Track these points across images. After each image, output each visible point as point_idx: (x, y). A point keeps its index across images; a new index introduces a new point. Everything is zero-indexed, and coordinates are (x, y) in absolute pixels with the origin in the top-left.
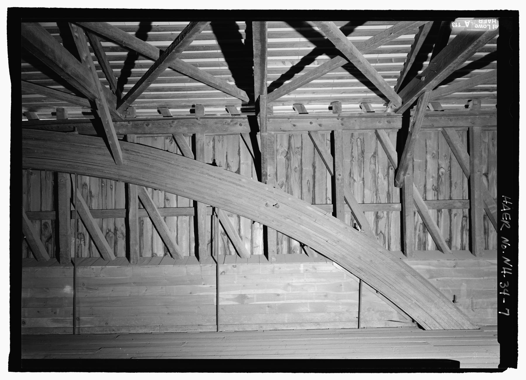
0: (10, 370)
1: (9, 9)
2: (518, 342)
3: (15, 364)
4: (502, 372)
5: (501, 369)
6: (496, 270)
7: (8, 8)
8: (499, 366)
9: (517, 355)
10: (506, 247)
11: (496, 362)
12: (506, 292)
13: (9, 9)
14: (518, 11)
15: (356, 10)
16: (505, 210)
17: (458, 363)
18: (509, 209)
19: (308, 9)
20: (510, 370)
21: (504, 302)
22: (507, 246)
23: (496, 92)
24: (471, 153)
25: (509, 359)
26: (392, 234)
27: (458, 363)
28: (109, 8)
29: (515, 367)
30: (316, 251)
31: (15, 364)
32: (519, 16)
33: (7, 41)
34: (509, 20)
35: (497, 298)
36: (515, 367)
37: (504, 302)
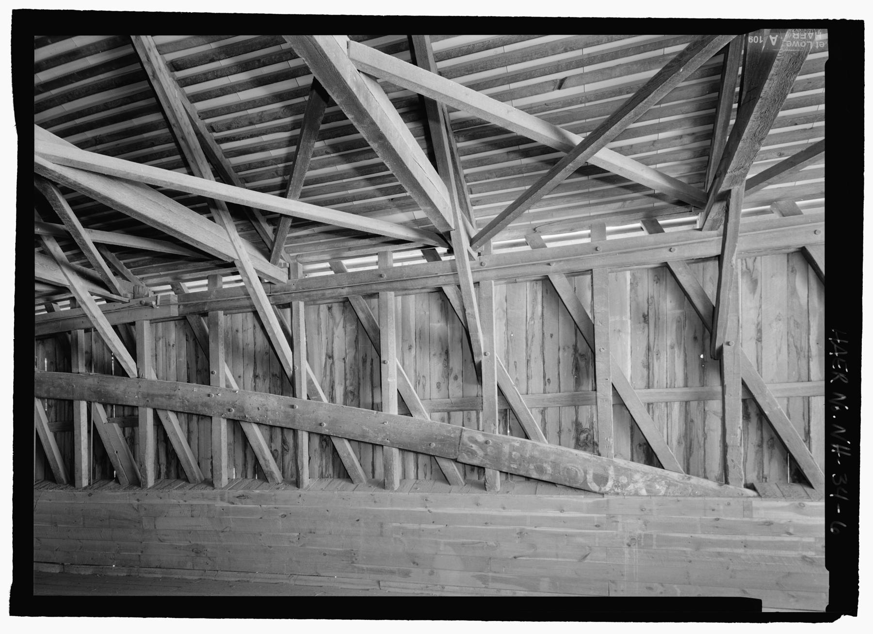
0: (12, 613)
1: (15, 12)
3: (24, 602)
4: (832, 621)
5: (829, 616)
6: (824, 523)
7: (14, 11)
9: (857, 594)
11: (821, 604)
13: (15, 12)
17: (758, 603)
18: (846, 353)
19: (513, 16)
20: (845, 619)
21: (839, 511)
22: (842, 408)
23: (822, 107)
24: (439, 165)
25: (843, 599)
26: (677, 371)
27: (758, 603)
29: (855, 614)
31: (24, 602)
33: (10, 65)
34: (847, 37)
35: (824, 518)
36: (855, 614)
37: (839, 511)
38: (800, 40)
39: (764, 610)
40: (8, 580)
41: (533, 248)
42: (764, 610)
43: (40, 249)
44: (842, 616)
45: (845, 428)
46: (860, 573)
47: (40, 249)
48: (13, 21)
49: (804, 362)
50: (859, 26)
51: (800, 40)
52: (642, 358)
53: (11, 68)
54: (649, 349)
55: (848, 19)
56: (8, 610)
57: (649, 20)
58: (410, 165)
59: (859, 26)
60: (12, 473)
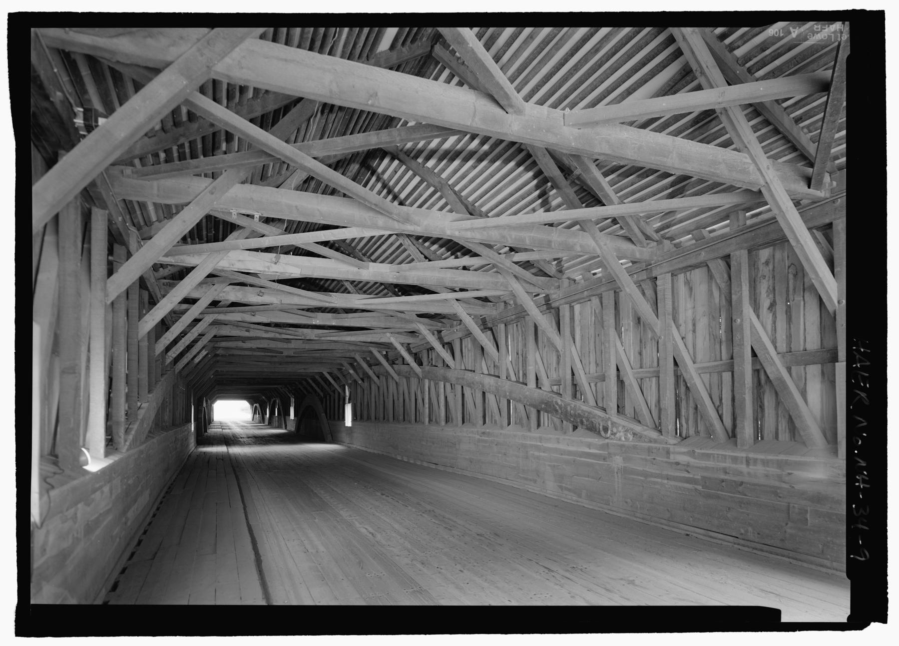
1: (11, 15)
2: (888, 578)
4: (862, 629)
9: (886, 601)
13: (11, 15)
17: (777, 613)
19: (523, 11)
20: (874, 626)
25: (869, 606)
29: (884, 620)
33: (7, 70)
34: (868, 29)
36: (884, 620)
39: (783, 621)
41: (633, 262)
44: (872, 623)
48: (9, 24)
49: (718, 346)
50: (879, 17)
52: (736, 361)
53: (7, 74)
54: (641, 342)
55: (868, 9)
56: (14, 630)
57: (664, 13)
58: (821, 275)
59: (879, 17)
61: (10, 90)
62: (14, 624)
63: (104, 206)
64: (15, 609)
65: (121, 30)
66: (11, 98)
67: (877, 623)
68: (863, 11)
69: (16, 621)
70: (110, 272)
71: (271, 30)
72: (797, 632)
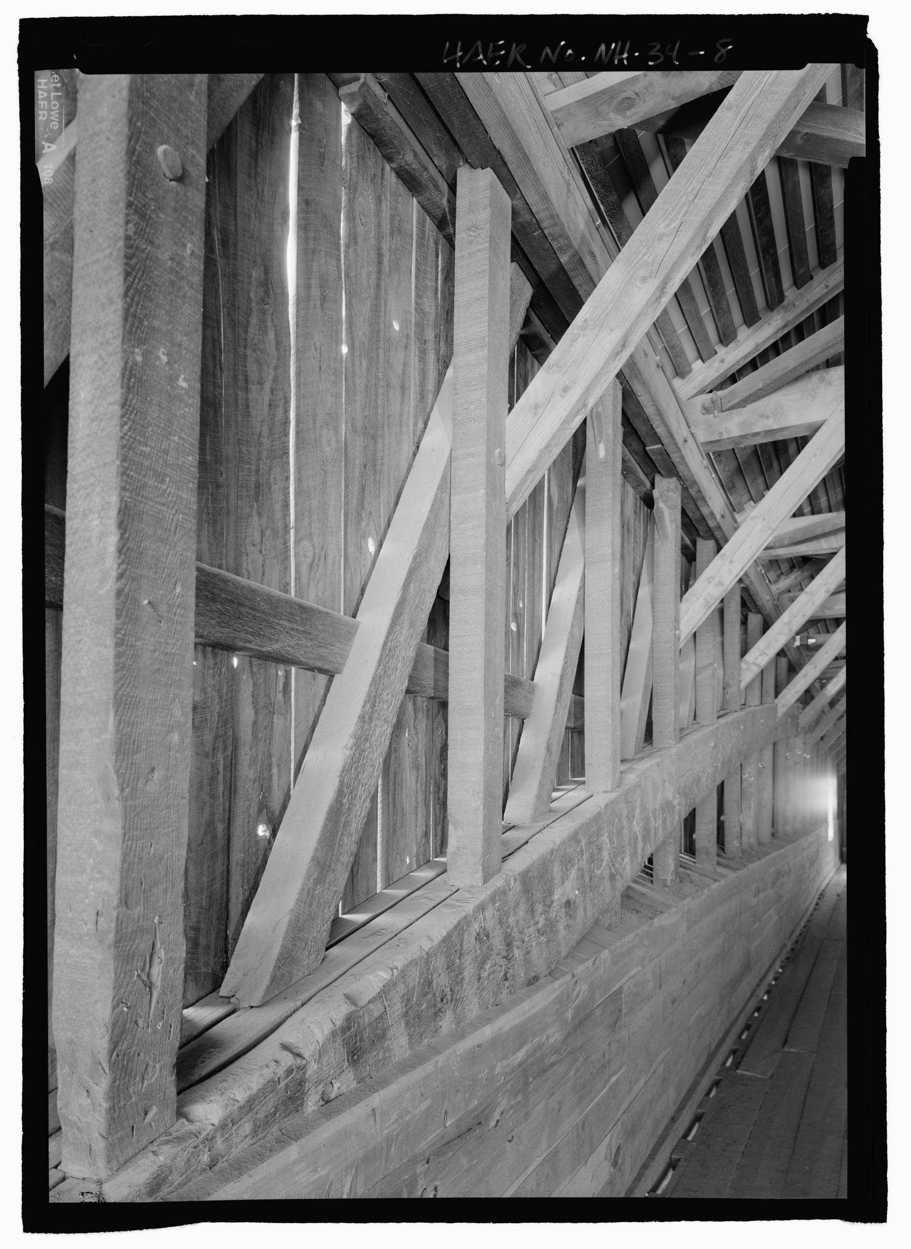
2: (805, 13)
3: (865, 1201)
4: (877, 51)
7: (26, 1230)
8: (860, 66)
10: (570, 51)
12: (672, 50)
13: (26, 1230)
14: (885, 1221)
15: (141, 1228)
16: (481, 57)
17: (854, 161)
18: (479, 43)
19: (21, 519)
20: (873, 32)
21: (702, 53)
28: (21, 991)
29: (865, 19)
30: (583, 587)
31: (865, 1201)
32: (32, 19)
34: (47, 45)
36: (865, 19)
37: (702, 53)
38: (50, 110)
40: (836, 1225)
42: (864, 154)
43: (834, 98)
44: (869, 36)
45: (543, 48)
46: (598, 13)
47: (834, 98)
50: (28, 27)
51: (50, 110)
55: (17, 42)
56: (878, 1225)
59: (28, 27)
60: (683, 1222)
61: (130, 1230)
62: (869, 1225)
63: (672, 471)
64: (848, 1224)
65: (50, 1106)
66: (141, 1229)
67: (868, 30)
68: (46, 1233)
69: (865, 1222)
70: (744, 652)
71: (48, 612)
72: (881, 140)
